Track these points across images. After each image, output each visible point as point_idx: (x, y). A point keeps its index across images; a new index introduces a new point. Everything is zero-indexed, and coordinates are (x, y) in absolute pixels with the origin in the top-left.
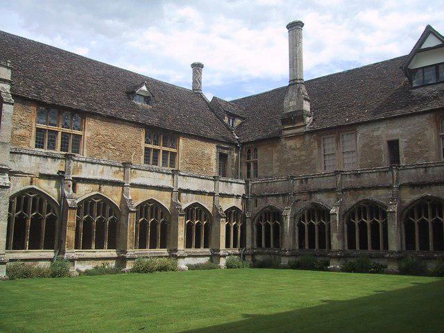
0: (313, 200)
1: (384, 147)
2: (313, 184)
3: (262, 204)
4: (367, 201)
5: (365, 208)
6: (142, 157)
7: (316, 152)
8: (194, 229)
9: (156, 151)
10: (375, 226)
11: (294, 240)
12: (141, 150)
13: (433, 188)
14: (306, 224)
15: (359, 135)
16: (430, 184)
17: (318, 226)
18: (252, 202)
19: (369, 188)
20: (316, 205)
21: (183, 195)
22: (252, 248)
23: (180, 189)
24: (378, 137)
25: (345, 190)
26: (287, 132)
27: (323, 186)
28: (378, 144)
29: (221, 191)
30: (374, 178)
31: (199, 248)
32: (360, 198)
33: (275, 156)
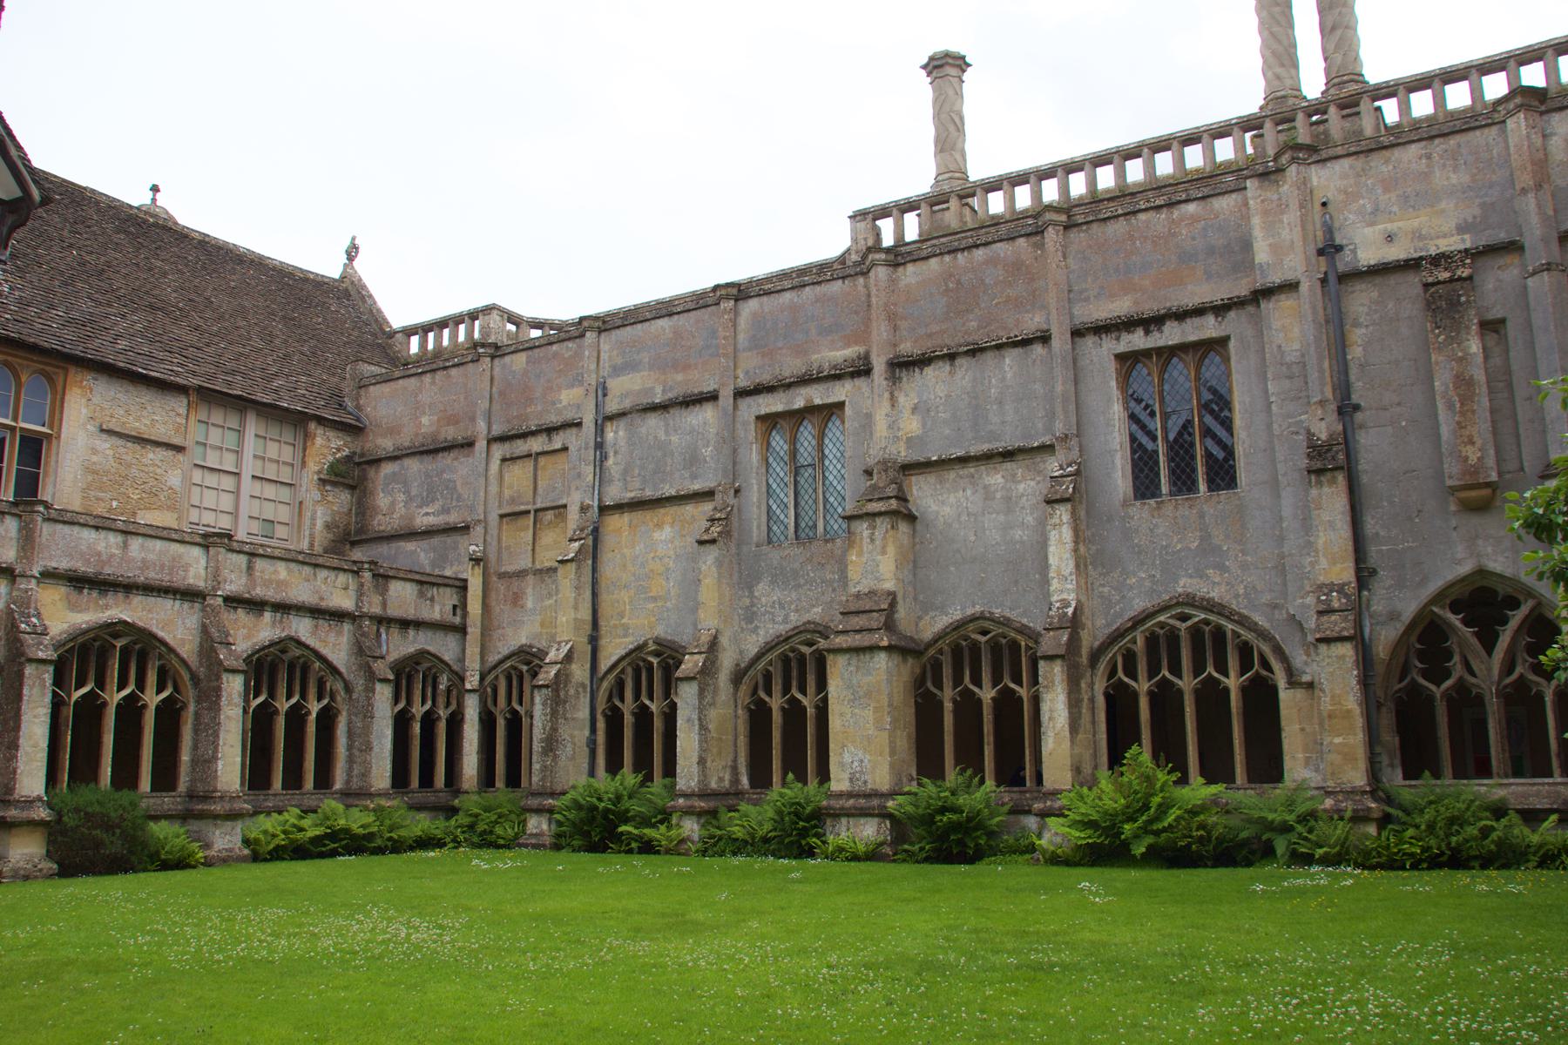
1: (564, 502)
10: (794, 712)
13: (137, 600)
16: (128, 588)
17: (1199, 694)
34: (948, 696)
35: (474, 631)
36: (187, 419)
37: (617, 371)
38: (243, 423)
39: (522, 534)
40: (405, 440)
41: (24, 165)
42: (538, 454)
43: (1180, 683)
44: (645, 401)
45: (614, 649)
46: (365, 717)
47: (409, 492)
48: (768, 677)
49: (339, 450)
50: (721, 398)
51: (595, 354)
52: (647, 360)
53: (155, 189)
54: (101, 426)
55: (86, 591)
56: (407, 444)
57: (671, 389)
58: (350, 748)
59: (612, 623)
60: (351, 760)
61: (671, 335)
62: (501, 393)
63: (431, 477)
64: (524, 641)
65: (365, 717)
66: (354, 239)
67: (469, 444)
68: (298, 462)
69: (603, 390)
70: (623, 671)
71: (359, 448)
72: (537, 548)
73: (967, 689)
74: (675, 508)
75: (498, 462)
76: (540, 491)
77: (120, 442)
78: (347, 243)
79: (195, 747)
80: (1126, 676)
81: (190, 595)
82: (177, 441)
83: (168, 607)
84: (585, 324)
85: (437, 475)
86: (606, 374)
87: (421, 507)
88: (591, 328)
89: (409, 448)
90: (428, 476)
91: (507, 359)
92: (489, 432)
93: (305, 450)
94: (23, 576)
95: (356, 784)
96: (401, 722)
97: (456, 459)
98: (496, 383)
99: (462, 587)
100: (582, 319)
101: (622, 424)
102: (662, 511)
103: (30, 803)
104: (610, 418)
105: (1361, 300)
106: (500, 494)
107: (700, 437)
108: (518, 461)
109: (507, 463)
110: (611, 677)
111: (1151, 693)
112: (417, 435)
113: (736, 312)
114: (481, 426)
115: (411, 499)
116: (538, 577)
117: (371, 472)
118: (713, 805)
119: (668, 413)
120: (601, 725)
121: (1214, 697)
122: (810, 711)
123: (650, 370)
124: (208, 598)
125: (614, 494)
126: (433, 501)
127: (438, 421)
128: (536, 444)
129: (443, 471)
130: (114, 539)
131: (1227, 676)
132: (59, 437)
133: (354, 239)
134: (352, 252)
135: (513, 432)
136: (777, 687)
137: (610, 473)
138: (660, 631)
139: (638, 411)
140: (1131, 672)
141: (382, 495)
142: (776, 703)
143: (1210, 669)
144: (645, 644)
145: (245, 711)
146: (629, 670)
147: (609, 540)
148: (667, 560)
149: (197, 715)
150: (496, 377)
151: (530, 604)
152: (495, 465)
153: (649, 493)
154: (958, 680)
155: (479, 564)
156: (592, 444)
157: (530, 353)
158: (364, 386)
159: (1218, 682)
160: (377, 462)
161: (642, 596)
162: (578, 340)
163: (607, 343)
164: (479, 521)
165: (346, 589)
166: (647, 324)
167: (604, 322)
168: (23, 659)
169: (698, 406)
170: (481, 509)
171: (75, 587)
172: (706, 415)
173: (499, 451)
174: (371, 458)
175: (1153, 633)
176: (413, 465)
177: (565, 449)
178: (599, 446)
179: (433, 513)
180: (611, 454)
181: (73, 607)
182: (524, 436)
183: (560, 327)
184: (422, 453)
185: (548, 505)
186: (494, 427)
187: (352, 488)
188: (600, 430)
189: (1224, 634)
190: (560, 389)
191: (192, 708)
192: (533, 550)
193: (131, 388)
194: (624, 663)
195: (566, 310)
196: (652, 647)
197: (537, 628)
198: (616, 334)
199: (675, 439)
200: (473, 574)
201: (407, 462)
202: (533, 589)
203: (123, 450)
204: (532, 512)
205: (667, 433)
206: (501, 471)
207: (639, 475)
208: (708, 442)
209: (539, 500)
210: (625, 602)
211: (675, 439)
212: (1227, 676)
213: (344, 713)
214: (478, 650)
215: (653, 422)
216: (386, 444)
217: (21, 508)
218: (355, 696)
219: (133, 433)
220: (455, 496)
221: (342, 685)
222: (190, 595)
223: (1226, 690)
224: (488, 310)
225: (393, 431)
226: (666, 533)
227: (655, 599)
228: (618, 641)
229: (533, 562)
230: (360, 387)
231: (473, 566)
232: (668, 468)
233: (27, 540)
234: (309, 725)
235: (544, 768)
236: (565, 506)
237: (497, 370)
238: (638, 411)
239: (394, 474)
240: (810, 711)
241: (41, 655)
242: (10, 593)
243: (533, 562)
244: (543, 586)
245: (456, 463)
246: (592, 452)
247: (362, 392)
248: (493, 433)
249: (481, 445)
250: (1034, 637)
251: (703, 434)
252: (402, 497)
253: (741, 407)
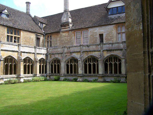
0: (72, 56)
1: (98, 36)
2: (72, 50)
3: (53, 57)
4: (91, 56)
5: (91, 59)
6: (6, 39)
7: (73, 37)
8: (13, 66)
9: (12, 37)
11: (83, 71)
12: (5, 36)
13: (115, 52)
14: (69, 64)
15: (89, 32)
18: (49, 56)
19: (92, 51)
20: (73, 58)
21: (22, 54)
22: (49, 74)
23: (21, 52)
24: (96, 33)
25: (84, 52)
26: (62, 30)
28: (96, 35)
29: (37, 52)
30: (94, 48)
31: (29, 74)
32: (89, 55)
33: (58, 39)
48: (86, 61)
53: (28, 3)
73: (111, 62)
83: (96, 53)
96: (40, 66)
111: (114, 64)
118: (82, 76)
120: (66, 66)
130: (111, 45)
136: (88, 62)
142: (69, 64)
145: (4, 65)
181: (108, 53)
241: (2, 60)
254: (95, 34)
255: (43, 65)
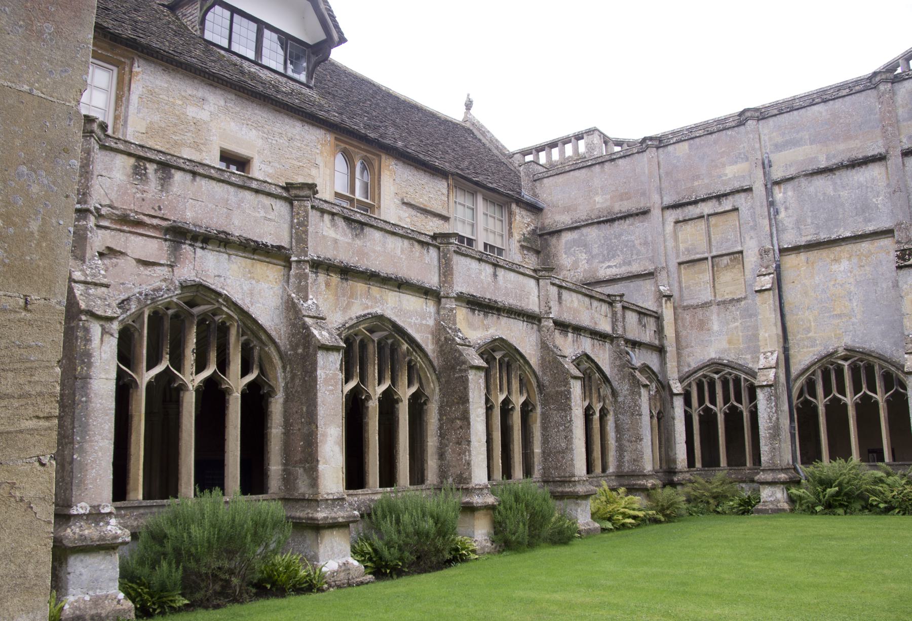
8: (373, 406)
10: (733, 417)
27: (238, 228)
34: (821, 402)
35: (671, 349)
36: (448, 196)
37: (778, 147)
38: (474, 202)
39: (701, 276)
40: (582, 214)
41: (329, 15)
42: (709, 215)
43: (845, 399)
44: (811, 167)
45: (803, 358)
46: (633, 414)
47: (591, 253)
49: (528, 225)
50: (900, 153)
51: (757, 136)
52: (807, 137)
54: (402, 199)
55: (476, 312)
56: (583, 218)
57: (834, 156)
58: (618, 440)
59: (799, 336)
60: (620, 449)
61: (829, 116)
62: (667, 174)
63: (610, 240)
64: (713, 355)
65: (633, 414)
66: (468, 95)
67: (645, 213)
68: (506, 233)
69: (766, 165)
70: (813, 373)
71: (539, 224)
72: (716, 285)
73: (707, 407)
74: (850, 246)
75: (672, 224)
76: (714, 242)
77: (413, 212)
78: (464, 99)
79: (545, 441)
80: (810, 396)
81: (532, 318)
82: (444, 213)
84: (748, 114)
85: (615, 237)
86: (768, 151)
87: (603, 262)
88: (752, 118)
89: (586, 220)
90: (606, 238)
91: (670, 148)
92: (662, 203)
93: (510, 224)
94: (447, 297)
95: (627, 468)
97: (632, 224)
98: (662, 167)
99: (658, 318)
100: (645, 139)
101: (789, 187)
102: (838, 249)
103: (480, 490)
104: (777, 183)
105: (779, 194)
106: (677, 247)
107: (869, 190)
108: (690, 222)
109: (679, 224)
110: (802, 380)
112: (592, 210)
113: (893, 93)
114: (656, 198)
115: (593, 257)
116: (722, 306)
117: (553, 240)
119: (835, 174)
121: (867, 408)
122: (746, 415)
123: (811, 144)
124: (543, 320)
125: (789, 239)
126: (614, 256)
127: (612, 198)
128: (706, 208)
129: (621, 235)
131: (845, 396)
132: (379, 207)
133: (468, 95)
134: (469, 105)
135: (684, 201)
137: (783, 224)
138: (848, 340)
139: (806, 175)
140: (813, 394)
141: (564, 256)
143: (865, 389)
144: (836, 352)
146: (819, 373)
147: (788, 275)
148: (848, 286)
149: (545, 417)
150: (662, 163)
151: (716, 327)
152: (670, 227)
153: (823, 236)
154: (827, 391)
155: (670, 300)
156: (765, 203)
157: (692, 141)
158: (538, 180)
159: (840, 400)
160: (558, 232)
161: (826, 315)
162: (736, 129)
163: (767, 128)
164: (663, 268)
165: (606, 316)
166: (804, 110)
167: (660, 141)
168: (464, 367)
169: (864, 167)
170: (663, 259)
171: (471, 308)
172: (875, 171)
173: (671, 216)
174: (551, 230)
175: (700, 380)
176: (592, 233)
177: (736, 209)
178: (771, 204)
179: (615, 266)
180: (782, 210)
182: (695, 202)
183: (630, 144)
184: (599, 223)
185: (724, 252)
186: (665, 199)
187: (538, 252)
188: (769, 192)
189: (740, 379)
190: (724, 165)
191: (539, 410)
192: (714, 287)
193: (416, 173)
194: (816, 367)
195: (635, 134)
196: (842, 353)
197: (724, 345)
198: (771, 121)
199: (844, 194)
200: (666, 308)
201: (585, 230)
202: (718, 315)
203: (416, 219)
204: (710, 259)
205: (835, 190)
206: (675, 231)
207: (812, 223)
208: (879, 193)
209: (714, 249)
210: (810, 320)
211: (844, 194)
212: (845, 396)
213: (611, 413)
214: (675, 364)
215: (820, 182)
216: (564, 219)
217: (439, 241)
218: (620, 399)
219: (422, 206)
220: (635, 252)
221: (610, 390)
222: (532, 318)
223: (845, 405)
224: (590, 132)
225: (567, 209)
226: (844, 265)
227: (839, 316)
228: (805, 350)
229: (715, 296)
230: (535, 181)
231: (666, 301)
232: (841, 216)
233: (446, 270)
234: (594, 423)
235: (773, 450)
236: (741, 252)
237: (662, 157)
238: (806, 175)
239: (574, 240)
240: (746, 415)
242: (438, 312)
243: (715, 296)
244: (728, 313)
245: (632, 228)
246: (766, 209)
247: (537, 184)
248: (664, 203)
249: (656, 213)
250: (753, 374)
251: (872, 188)
252: (583, 256)
253: (907, 164)
254: (189, 137)
255: (506, 402)
